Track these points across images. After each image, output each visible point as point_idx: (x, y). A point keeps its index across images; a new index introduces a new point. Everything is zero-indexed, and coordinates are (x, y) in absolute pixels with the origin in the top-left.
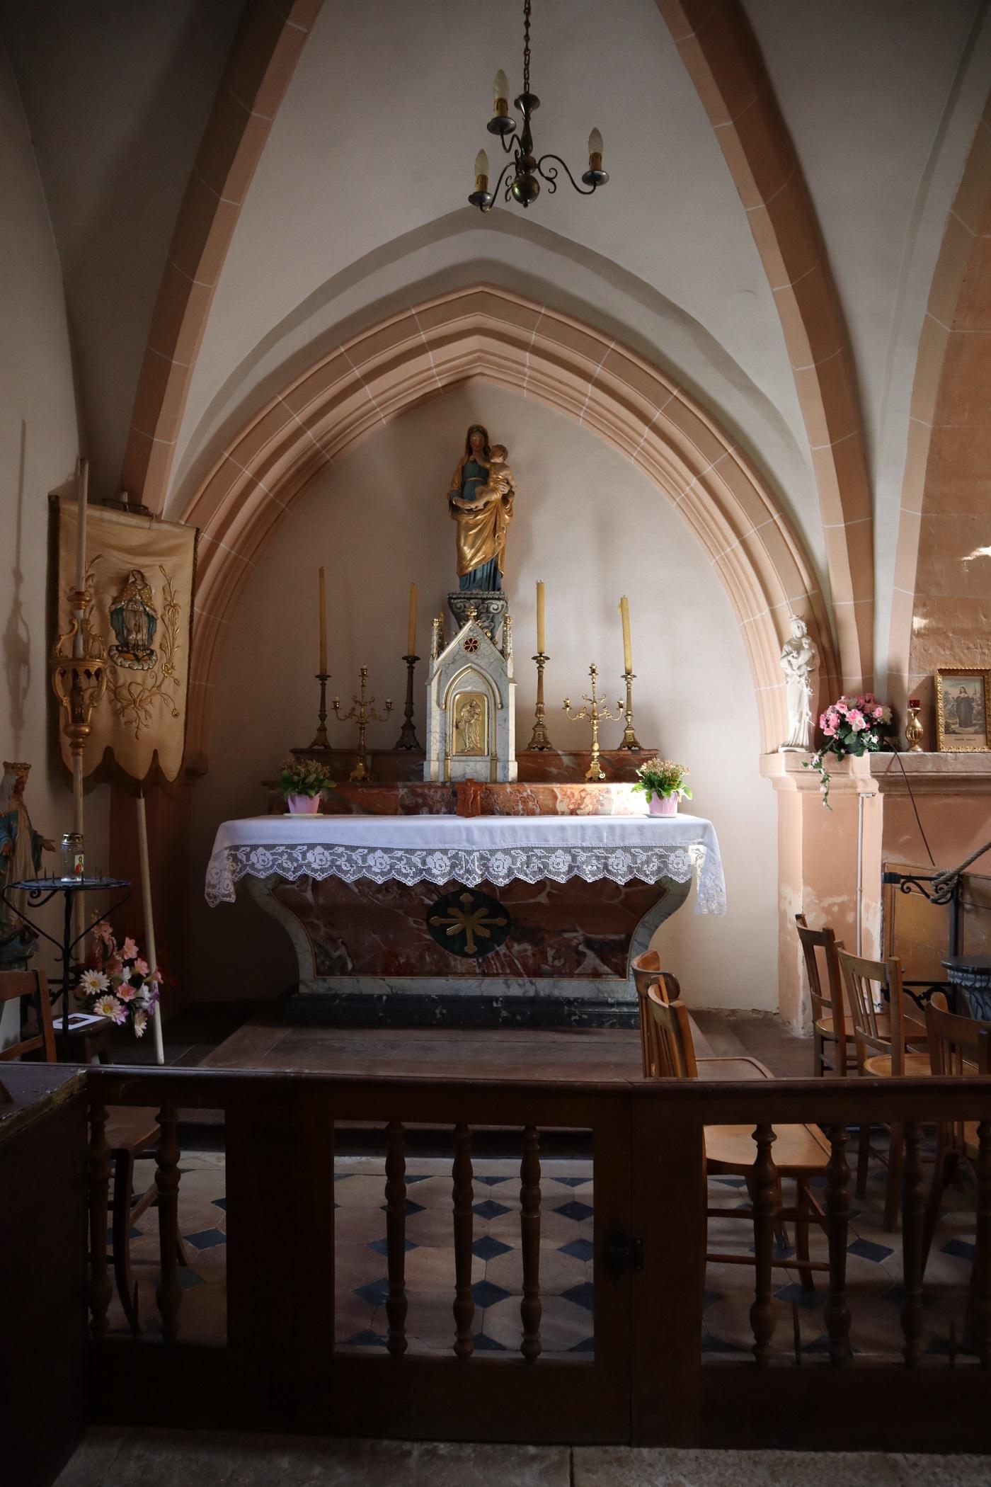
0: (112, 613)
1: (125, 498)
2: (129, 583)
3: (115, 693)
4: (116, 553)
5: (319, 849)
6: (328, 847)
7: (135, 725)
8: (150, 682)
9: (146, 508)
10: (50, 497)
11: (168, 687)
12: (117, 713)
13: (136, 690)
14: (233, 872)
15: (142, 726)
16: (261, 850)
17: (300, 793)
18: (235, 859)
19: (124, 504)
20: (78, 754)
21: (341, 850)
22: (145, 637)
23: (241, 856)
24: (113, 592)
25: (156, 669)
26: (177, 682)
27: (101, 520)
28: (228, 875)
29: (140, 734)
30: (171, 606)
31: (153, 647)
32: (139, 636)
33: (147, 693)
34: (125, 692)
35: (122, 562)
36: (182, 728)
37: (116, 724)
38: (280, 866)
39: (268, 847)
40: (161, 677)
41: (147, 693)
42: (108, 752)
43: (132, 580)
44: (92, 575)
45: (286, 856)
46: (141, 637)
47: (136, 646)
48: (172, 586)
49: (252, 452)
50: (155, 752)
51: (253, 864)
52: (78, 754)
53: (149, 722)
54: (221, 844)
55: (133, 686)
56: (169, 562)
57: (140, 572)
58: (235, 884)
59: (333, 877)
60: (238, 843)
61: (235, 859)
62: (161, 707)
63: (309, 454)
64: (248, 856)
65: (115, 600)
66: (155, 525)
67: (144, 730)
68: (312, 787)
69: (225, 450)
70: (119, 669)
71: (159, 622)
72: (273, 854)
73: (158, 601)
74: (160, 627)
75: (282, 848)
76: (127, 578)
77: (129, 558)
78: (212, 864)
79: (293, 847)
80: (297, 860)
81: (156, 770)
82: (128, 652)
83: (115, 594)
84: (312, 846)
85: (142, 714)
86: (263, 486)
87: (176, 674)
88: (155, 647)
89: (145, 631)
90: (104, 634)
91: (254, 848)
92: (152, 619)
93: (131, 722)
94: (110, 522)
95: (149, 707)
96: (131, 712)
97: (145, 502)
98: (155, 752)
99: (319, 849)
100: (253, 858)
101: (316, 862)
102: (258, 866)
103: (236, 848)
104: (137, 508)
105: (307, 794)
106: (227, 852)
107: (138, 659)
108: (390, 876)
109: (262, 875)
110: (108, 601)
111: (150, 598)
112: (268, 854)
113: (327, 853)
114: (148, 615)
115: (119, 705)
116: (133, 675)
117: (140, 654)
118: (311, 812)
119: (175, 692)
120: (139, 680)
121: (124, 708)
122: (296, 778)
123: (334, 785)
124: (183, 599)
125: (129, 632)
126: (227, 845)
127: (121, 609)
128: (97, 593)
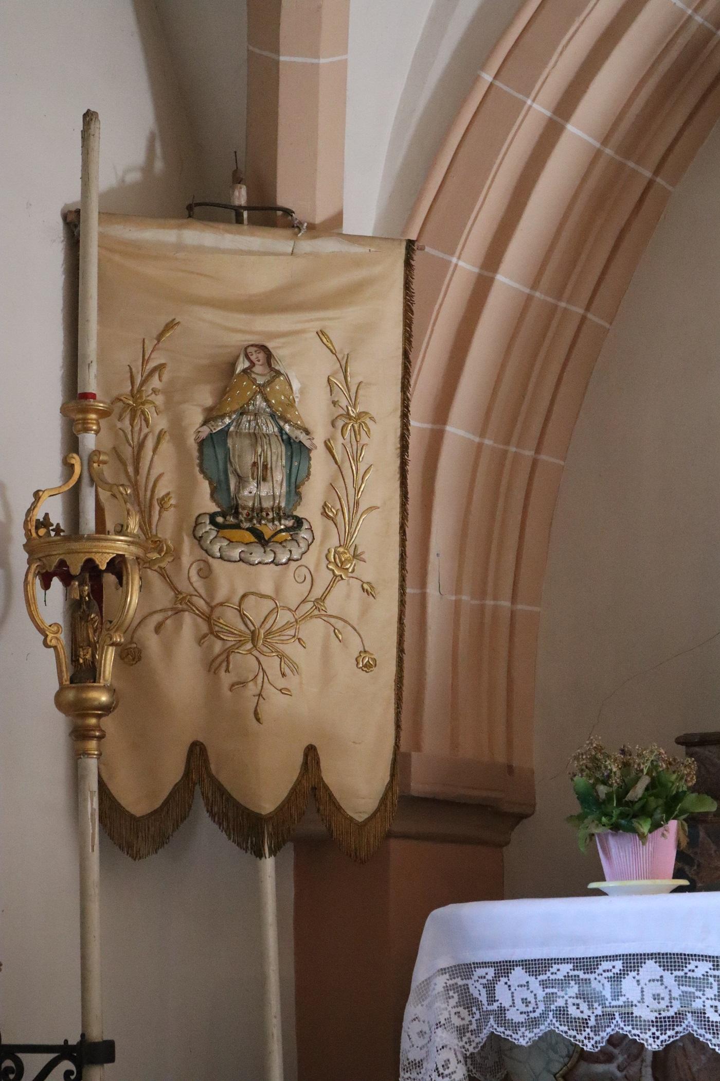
0: (201, 444)
1: (241, 196)
2: (244, 379)
3: (208, 619)
4: (209, 314)
5: (651, 969)
6: (672, 961)
7: (252, 689)
8: (294, 592)
9: (288, 212)
10: (65, 217)
11: (344, 599)
12: (214, 666)
13: (256, 611)
14: (462, 1031)
15: (269, 691)
16: (518, 975)
17: (616, 828)
18: (468, 1001)
19: (238, 211)
20: (86, 753)
21: (703, 968)
22: (281, 490)
23: (478, 991)
24: (205, 397)
25: (310, 560)
26: (369, 590)
27: (180, 247)
28: (443, 1036)
29: (266, 710)
30: (351, 420)
31: (300, 512)
32: (265, 491)
33: (284, 617)
34: (230, 617)
35: (218, 331)
36: (389, 693)
37: (213, 694)
38: (561, 1013)
39: (535, 967)
40: (324, 577)
41: (284, 617)
42: (197, 753)
43: (242, 365)
44: (160, 368)
45: (574, 989)
46: (270, 491)
47: (258, 512)
48: (344, 365)
49: (541, 61)
50: (311, 753)
51: (502, 1010)
52: (86, 753)
53: (292, 682)
54: (431, 961)
55: (251, 599)
56: (340, 322)
57: (263, 348)
58: (469, 1059)
59: (616, 1041)
60: (470, 957)
61: (468, 1001)
62: (326, 648)
63: (682, 41)
64: (490, 988)
65: (211, 416)
66: (306, 245)
67: (275, 703)
68: (644, 811)
69: (483, 66)
70: (216, 564)
71: (318, 457)
72: (544, 984)
73: (314, 411)
74: (320, 467)
75: (566, 968)
76: (233, 365)
77: (238, 320)
78: (412, 1009)
79: (589, 964)
80: (601, 1000)
81: (311, 784)
82: (237, 526)
83: (209, 402)
84: (633, 962)
85: (272, 664)
86: (579, 132)
87: (366, 571)
88: (309, 510)
89: (279, 476)
90: (186, 492)
91: (504, 968)
92: (297, 450)
93: (243, 683)
94: (200, 249)
95: (292, 649)
96: (243, 661)
97: (283, 200)
98: (311, 753)
99: (651, 969)
100: (503, 995)
101: (645, 999)
102: (513, 1015)
103: (466, 970)
104: (268, 214)
105: (634, 831)
106: (441, 982)
107: (262, 540)
108: (543, 1028)
109: (524, 1038)
110: (194, 417)
111: (291, 404)
112: (534, 983)
113: (669, 978)
114: (289, 442)
115: (218, 647)
116: (251, 579)
117: (268, 529)
118: (652, 875)
119: (365, 611)
120: (267, 587)
121: (228, 652)
122: (602, 790)
123: (710, 806)
124: (382, 403)
125: (242, 481)
126: (444, 962)
127: (225, 433)
128: (169, 403)
